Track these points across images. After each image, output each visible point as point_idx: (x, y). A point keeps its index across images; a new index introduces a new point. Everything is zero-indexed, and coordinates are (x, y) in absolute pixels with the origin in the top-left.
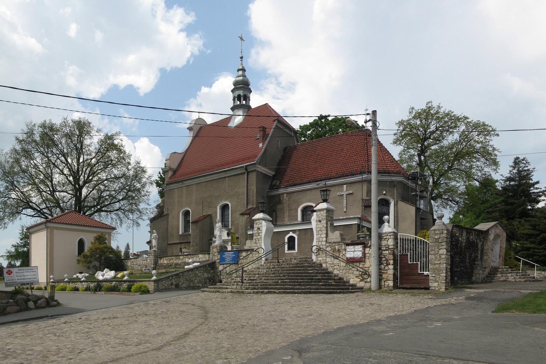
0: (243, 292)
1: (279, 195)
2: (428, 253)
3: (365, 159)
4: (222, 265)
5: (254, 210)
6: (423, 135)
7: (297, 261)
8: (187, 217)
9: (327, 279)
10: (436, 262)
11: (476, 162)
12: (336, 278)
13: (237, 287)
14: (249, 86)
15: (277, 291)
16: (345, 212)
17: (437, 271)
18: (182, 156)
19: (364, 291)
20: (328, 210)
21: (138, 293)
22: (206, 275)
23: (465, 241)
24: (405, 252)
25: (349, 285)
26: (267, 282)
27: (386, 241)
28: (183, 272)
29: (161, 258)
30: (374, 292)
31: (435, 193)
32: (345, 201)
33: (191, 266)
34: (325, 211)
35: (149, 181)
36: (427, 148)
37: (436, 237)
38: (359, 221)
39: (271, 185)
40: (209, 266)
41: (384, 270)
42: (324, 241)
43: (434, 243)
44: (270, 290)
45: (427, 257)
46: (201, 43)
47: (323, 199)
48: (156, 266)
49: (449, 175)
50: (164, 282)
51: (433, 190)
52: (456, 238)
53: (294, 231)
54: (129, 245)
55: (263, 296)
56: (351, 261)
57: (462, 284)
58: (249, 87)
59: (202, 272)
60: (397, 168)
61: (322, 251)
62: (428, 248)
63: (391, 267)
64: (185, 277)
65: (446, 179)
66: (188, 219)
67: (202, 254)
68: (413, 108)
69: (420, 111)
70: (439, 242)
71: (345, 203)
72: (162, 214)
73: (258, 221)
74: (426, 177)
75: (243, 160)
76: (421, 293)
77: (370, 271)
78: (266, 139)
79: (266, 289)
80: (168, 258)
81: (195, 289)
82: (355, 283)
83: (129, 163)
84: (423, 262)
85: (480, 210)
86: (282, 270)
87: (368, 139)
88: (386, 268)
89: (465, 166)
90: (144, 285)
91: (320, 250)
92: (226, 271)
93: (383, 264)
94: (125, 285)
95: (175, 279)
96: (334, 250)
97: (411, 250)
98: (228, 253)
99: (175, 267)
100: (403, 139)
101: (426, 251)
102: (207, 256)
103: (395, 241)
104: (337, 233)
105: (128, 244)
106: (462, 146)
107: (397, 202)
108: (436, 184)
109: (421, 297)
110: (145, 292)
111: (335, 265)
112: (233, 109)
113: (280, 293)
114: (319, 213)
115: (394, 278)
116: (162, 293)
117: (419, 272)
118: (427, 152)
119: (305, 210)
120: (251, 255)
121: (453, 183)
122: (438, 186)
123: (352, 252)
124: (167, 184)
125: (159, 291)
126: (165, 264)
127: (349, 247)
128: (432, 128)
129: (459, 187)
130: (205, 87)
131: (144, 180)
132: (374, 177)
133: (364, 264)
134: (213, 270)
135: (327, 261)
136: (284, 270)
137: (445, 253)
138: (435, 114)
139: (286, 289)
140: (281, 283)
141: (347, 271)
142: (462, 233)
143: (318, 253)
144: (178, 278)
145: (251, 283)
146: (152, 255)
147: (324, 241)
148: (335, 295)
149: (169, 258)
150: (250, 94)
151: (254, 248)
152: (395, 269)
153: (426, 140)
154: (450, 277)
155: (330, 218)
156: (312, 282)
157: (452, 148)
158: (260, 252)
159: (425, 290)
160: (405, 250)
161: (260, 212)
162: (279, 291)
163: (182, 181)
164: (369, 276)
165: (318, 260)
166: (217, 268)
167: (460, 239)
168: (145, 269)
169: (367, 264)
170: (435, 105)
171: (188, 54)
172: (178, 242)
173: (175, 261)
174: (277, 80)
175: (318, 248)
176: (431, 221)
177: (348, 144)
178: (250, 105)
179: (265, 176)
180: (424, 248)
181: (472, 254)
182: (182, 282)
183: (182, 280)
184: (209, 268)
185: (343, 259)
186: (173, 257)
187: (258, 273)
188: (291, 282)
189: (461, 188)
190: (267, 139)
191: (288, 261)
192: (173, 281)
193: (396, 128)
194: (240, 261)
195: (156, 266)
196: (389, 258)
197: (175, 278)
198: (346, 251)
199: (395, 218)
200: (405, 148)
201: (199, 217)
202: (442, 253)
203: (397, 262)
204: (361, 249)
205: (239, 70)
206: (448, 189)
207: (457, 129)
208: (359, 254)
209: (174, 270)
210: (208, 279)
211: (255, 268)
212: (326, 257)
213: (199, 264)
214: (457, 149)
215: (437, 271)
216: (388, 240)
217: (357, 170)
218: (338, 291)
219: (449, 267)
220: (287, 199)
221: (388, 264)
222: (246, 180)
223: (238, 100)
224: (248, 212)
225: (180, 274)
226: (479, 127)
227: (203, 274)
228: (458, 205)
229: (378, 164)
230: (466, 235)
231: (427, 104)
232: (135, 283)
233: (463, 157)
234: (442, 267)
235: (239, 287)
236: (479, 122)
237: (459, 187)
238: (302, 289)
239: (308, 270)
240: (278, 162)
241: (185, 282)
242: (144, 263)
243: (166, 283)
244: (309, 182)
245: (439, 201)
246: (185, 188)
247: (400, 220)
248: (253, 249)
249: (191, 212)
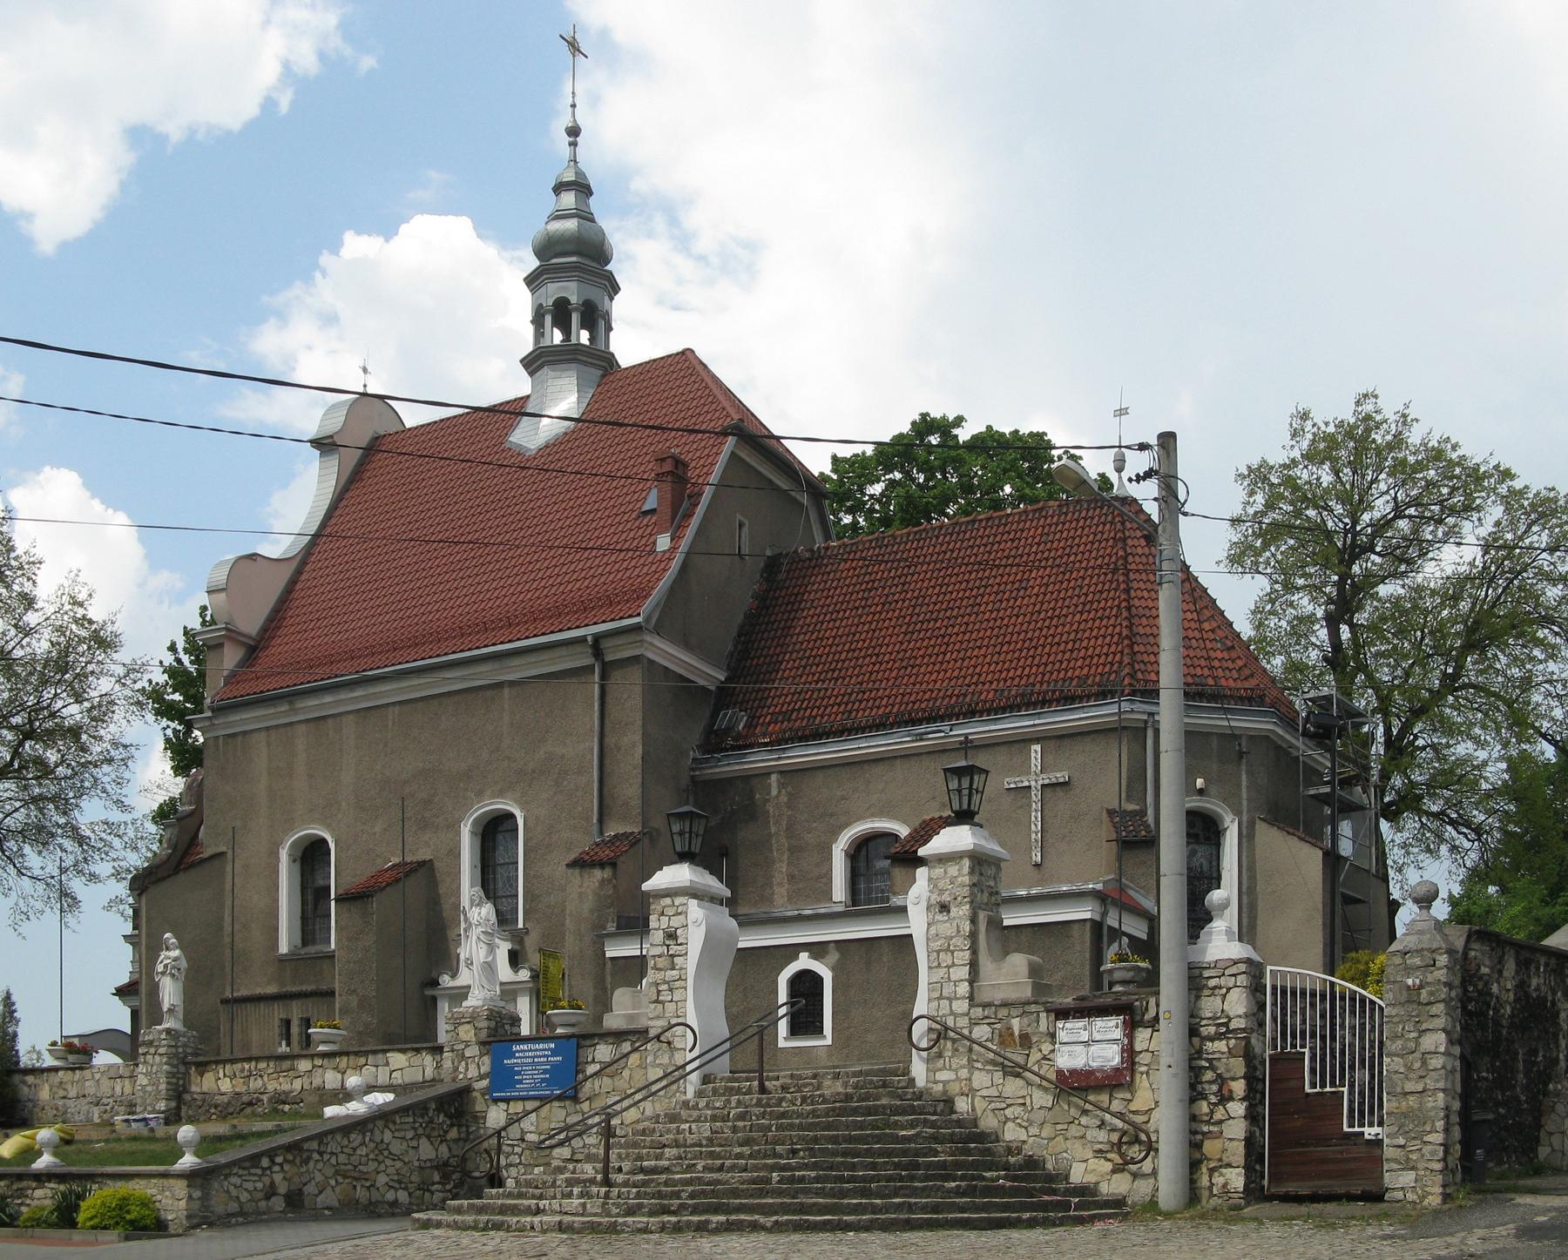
0: (613, 1229)
1: (747, 778)
2: (1381, 1049)
3: (1117, 630)
4: (503, 1106)
5: (632, 845)
6: (1346, 536)
7: (846, 1085)
8: (313, 870)
9: (975, 1165)
10: (1409, 1087)
11: (1546, 661)
12: (1012, 1160)
13: (584, 1205)
14: (608, 262)
15: (768, 1221)
16: (1037, 865)
17: (1411, 1122)
18: (287, 572)
19: (1129, 1213)
20: (979, 861)
21: (112, 1235)
22: (426, 1150)
23: (1512, 996)
24: (1294, 1046)
25: (1067, 1190)
26: (718, 1182)
27: (1219, 1000)
28: (320, 1137)
29: (202, 1067)
30: (1168, 1215)
31: (1392, 788)
32: (1036, 816)
33: (356, 1108)
34: (966, 863)
35: (128, 693)
36: (1362, 589)
37: (1410, 982)
38: (1098, 908)
39: (710, 731)
40: (438, 1110)
41: (1208, 1123)
42: (964, 998)
43: (1402, 1004)
44: (734, 1217)
45: (1374, 1066)
46: (331, 19)
47: (956, 806)
48: (178, 1108)
49: (1448, 711)
50: (234, 1180)
51: (1385, 776)
52: (1480, 987)
53: (817, 950)
54: (14, 998)
55: (705, 1243)
56: (1076, 1085)
57: (1501, 1177)
58: (608, 267)
59: (410, 1134)
60: (1252, 675)
61: (954, 1041)
62: (1381, 1025)
63: (1238, 1108)
64: (333, 1161)
65: (1435, 730)
66: (321, 883)
67: (403, 1051)
68: (1305, 416)
69: (1331, 429)
70: (1420, 1003)
71: (1036, 826)
72: (186, 853)
73: (668, 901)
74: (1361, 720)
75: (584, 610)
76: (1353, 1218)
77: (1151, 1126)
78: (689, 515)
79: (716, 1210)
80: (239, 1065)
81: (379, 1216)
82: (1091, 1179)
83: (28, 601)
84: (1362, 1086)
85: (1560, 865)
86: (780, 1128)
87: (1129, 542)
88: (1219, 1114)
89: (1506, 676)
90: (137, 1193)
91: (946, 1038)
92: (523, 1132)
93: (1205, 1098)
94: (43, 1197)
95: (286, 1167)
96: (1005, 1037)
97: (1313, 1035)
99: (276, 1110)
100: (1266, 546)
101: (1372, 1042)
102: (428, 1060)
103: (1254, 996)
104: (1018, 962)
105: (8, 996)
106: (1495, 589)
107: (1252, 824)
108: (1398, 749)
109: (1355, 1231)
110: (145, 1228)
112: (534, 363)
113: (778, 1228)
114: (938, 871)
115: (1248, 1155)
116: (228, 1233)
117: (1346, 1129)
118: (1360, 608)
119: (863, 853)
120: (634, 1059)
121: (1463, 748)
122: (1406, 759)
123: (1080, 1048)
124: (219, 710)
125: (211, 1225)
126: (225, 1099)
127: (1068, 1025)
128: (1382, 507)
129: (1485, 763)
130: (359, 233)
131: (103, 686)
132: (1169, 712)
133: (1128, 1096)
134: (460, 1126)
135: (976, 1085)
136: (791, 1127)
137: (1442, 1049)
138: (1391, 447)
139: (802, 1209)
140: (779, 1182)
141: (1059, 1127)
142: (1500, 962)
143: (935, 1049)
144: (298, 1161)
145: (645, 1183)
146: (162, 1050)
147: (964, 998)
148: (1015, 1234)
149: (243, 1070)
150: (612, 299)
151: (651, 1023)
152: (1253, 1117)
153: (1358, 557)
154: (1458, 1147)
155: (986, 894)
156: (912, 1178)
157: (1456, 598)
158: (678, 1043)
159: (1368, 1204)
160: (1294, 1037)
161: (676, 857)
162: (776, 1222)
163: (291, 696)
164: (1151, 1148)
165: (936, 1082)
166: (480, 1118)
167: (1495, 988)
168: (127, 1121)
169: (1142, 1100)
170: (1389, 409)
171: (267, 73)
172: (271, 989)
173: (271, 1082)
174: (674, 221)
175: (935, 1026)
176: (1384, 911)
177: (1047, 559)
178: (612, 349)
179: (685, 689)
180: (1363, 1026)
181: (1535, 1052)
182: (319, 1178)
183: (318, 1171)
184: (442, 1117)
185: (1042, 1078)
186: (262, 1065)
187: (676, 1141)
188: (824, 1179)
189: (1492, 769)
190: (691, 515)
191: (805, 1085)
192: (278, 1178)
193: (1239, 492)
194: (588, 1084)
195: (178, 1108)
196: (1228, 1071)
197: (285, 1160)
198: (1054, 1043)
199: (1245, 898)
200: (1277, 587)
201: (371, 871)
202: (1433, 1049)
203: (1260, 1087)
204: (1117, 1034)
205: (559, 188)
206: (1442, 772)
207: (1475, 519)
208: (1108, 1056)
209: (269, 1125)
210: (437, 1168)
211: (656, 1118)
212: (972, 1068)
213: (390, 1097)
214: (1474, 604)
215: (1411, 1122)
216: (1224, 996)
217: (1087, 677)
218: (1027, 1215)
219: (1456, 1105)
221: (1225, 1098)
223: (555, 324)
224: (606, 853)
225: (306, 1146)
226: (1554, 513)
227: (414, 1143)
228: (1479, 840)
229: (1188, 663)
230: (1517, 972)
231: (1358, 403)
232: (95, 1187)
233: (1497, 638)
234: (1430, 1105)
235: (593, 1206)
236: (1552, 494)
237: (1485, 763)
238: (875, 1209)
239: (896, 1125)
240: (742, 627)
241: (333, 1182)
242: (118, 1090)
243: (246, 1185)
244: (880, 726)
245: (1411, 823)
246: (302, 728)
247: (1260, 904)
248: (646, 1031)
249: (332, 846)
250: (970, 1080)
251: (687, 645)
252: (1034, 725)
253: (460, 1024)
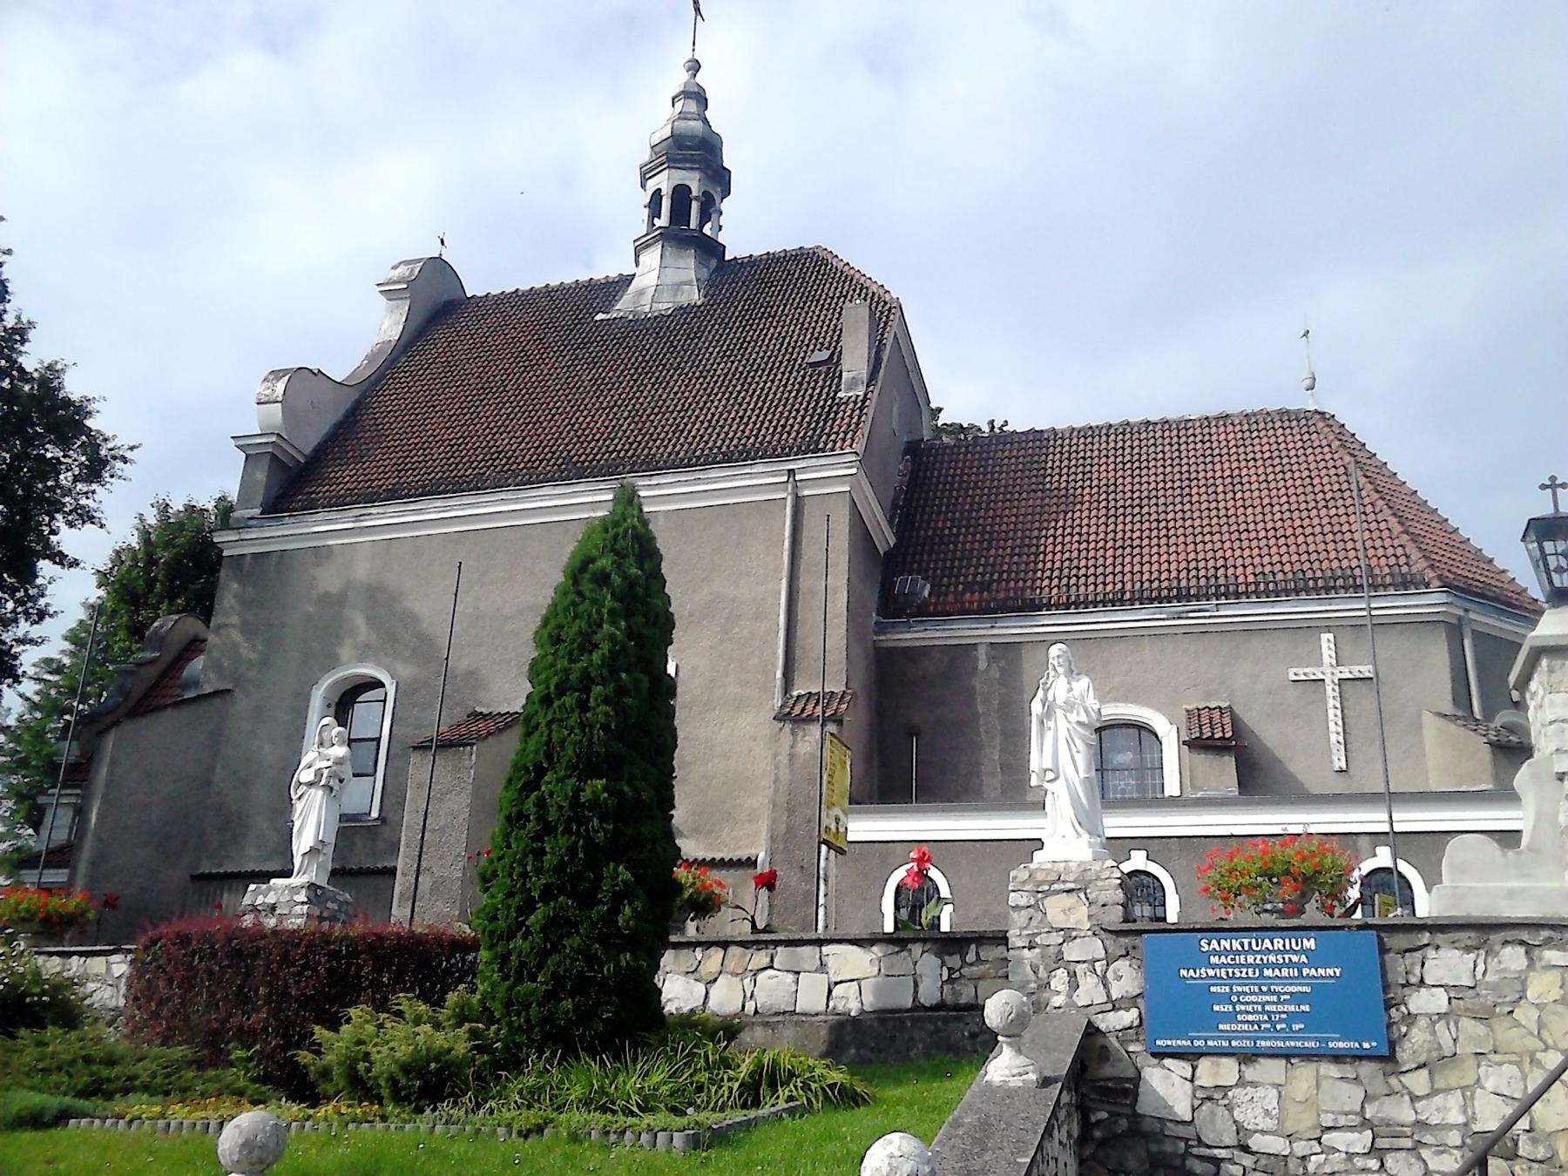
4: (1181, 1068)
18: (348, 399)
32: (1334, 715)
71: (1335, 727)
220: (995, 673)
252: (1327, 611)
253: (1047, 894)
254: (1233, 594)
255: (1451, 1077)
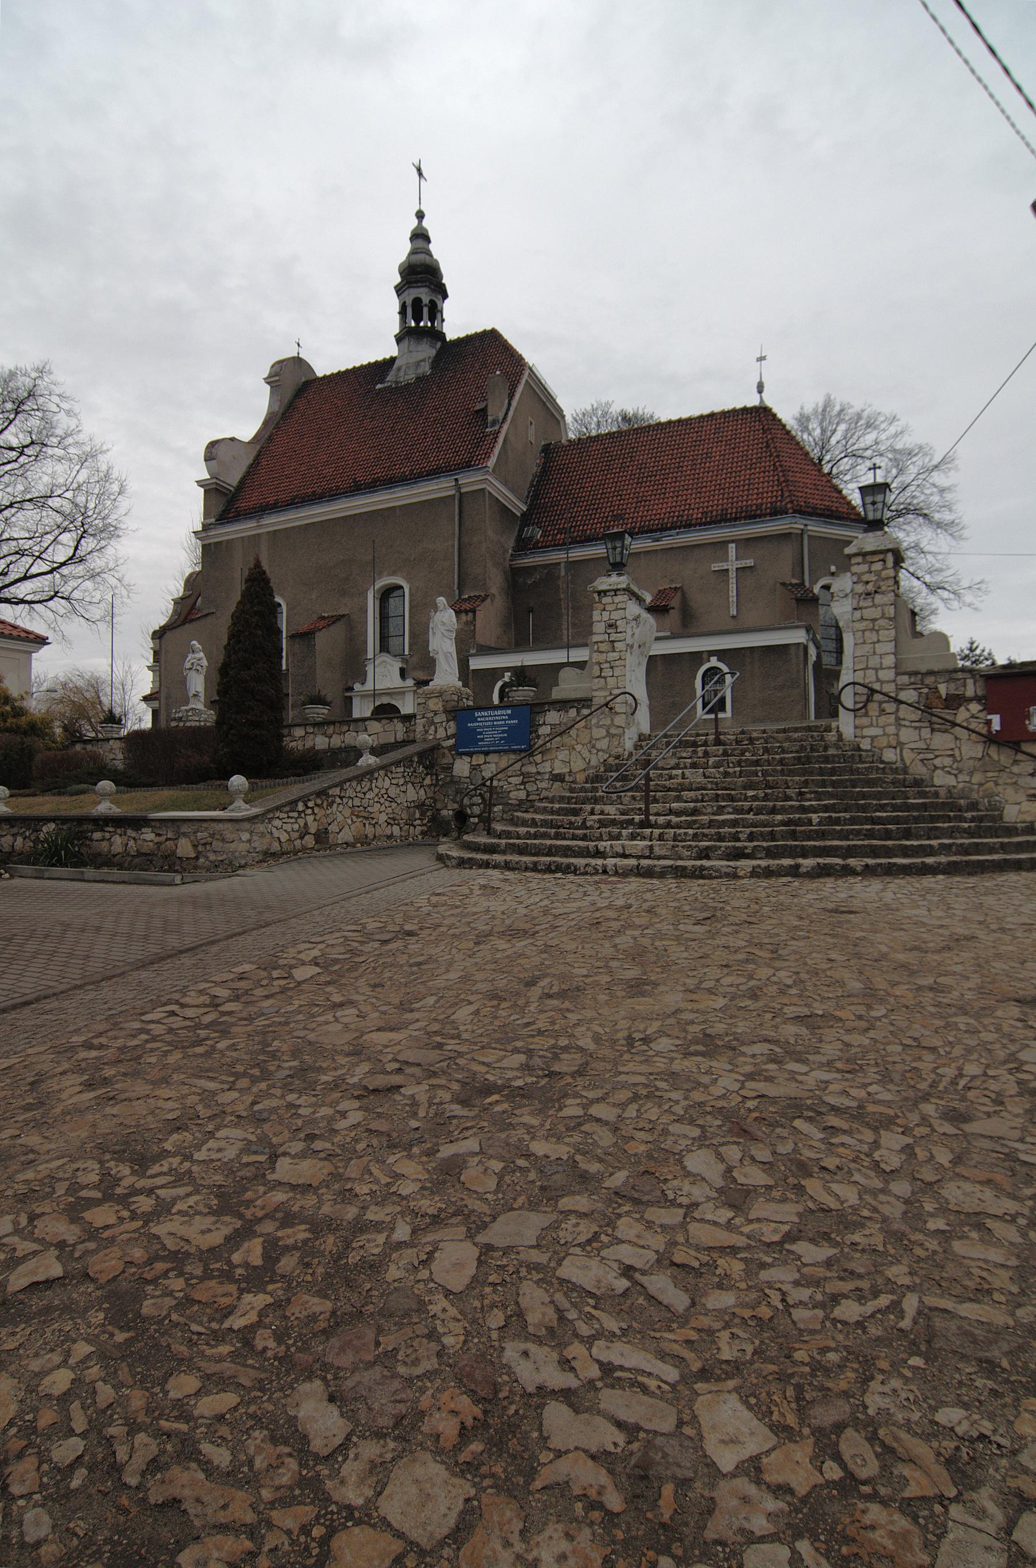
4: (467, 759)
13: (651, 847)
39: (519, 539)
50: (277, 823)
59: (401, 781)
95: (316, 810)
98: (492, 713)
111: (937, 753)
135: (902, 739)
140: (820, 824)
141: (990, 774)
151: (595, 694)
222: (457, 518)
225: (331, 792)
227: (403, 788)
250: (897, 735)
251: (505, 484)
254: (688, 525)
255: (547, 757)
